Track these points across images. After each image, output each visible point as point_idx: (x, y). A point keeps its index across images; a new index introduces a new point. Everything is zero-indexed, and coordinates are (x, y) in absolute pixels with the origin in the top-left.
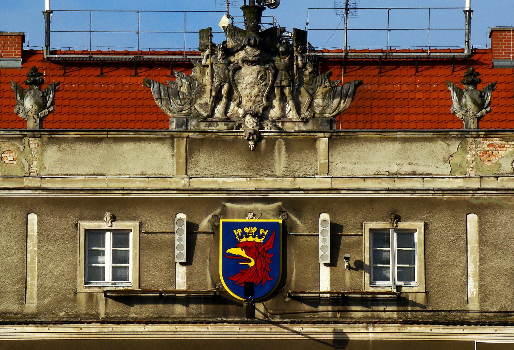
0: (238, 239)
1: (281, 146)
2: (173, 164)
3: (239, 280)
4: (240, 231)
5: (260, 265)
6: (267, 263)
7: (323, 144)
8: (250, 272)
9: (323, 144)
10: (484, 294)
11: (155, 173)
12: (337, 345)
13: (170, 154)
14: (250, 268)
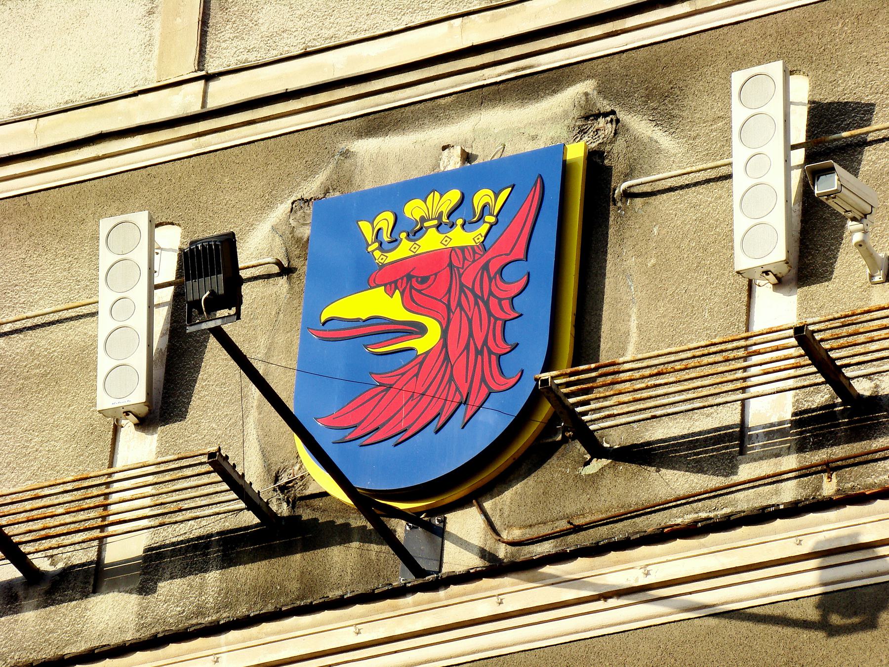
0: (377, 254)
2: (149, 44)
3: (362, 421)
4: (385, 220)
5: (465, 333)
6: (496, 319)
8: (417, 375)
11: (71, 97)
12: (835, 619)
13: (143, 10)
14: (421, 358)
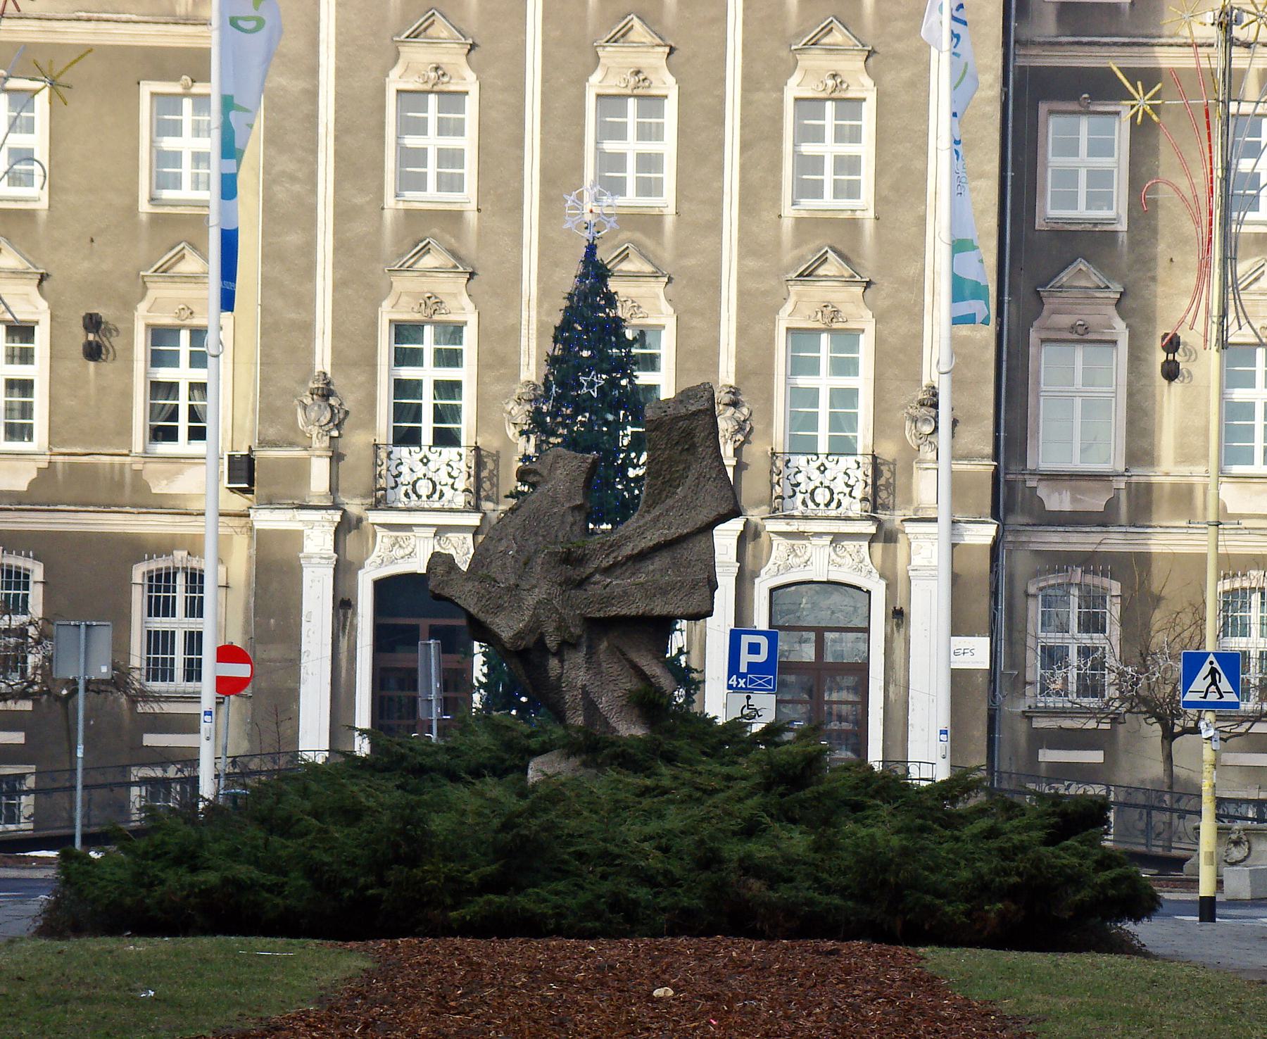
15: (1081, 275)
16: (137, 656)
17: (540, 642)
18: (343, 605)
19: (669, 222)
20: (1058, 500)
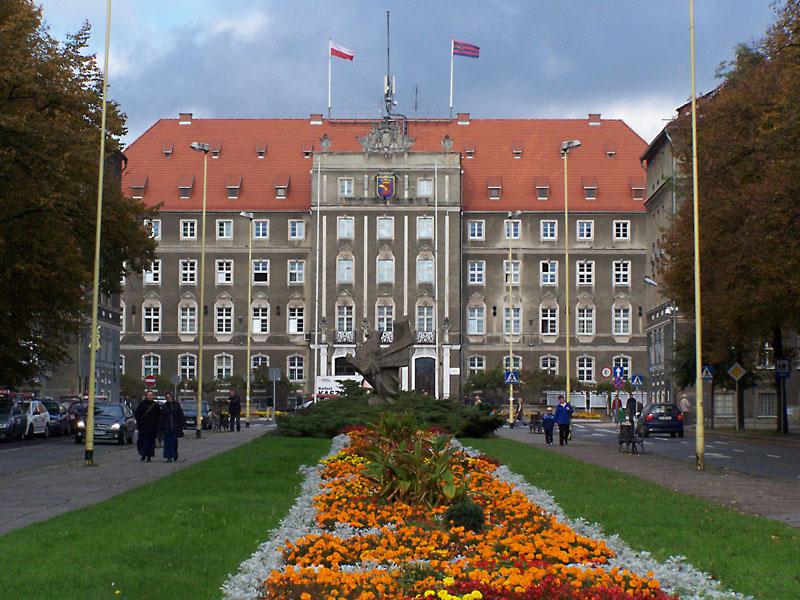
1: (394, 156)
7: (406, 155)
9: (406, 155)
10: (450, 197)
15: (476, 295)
16: (288, 375)
17: (371, 373)
18: (329, 364)
19: (394, 286)
20: (473, 340)
